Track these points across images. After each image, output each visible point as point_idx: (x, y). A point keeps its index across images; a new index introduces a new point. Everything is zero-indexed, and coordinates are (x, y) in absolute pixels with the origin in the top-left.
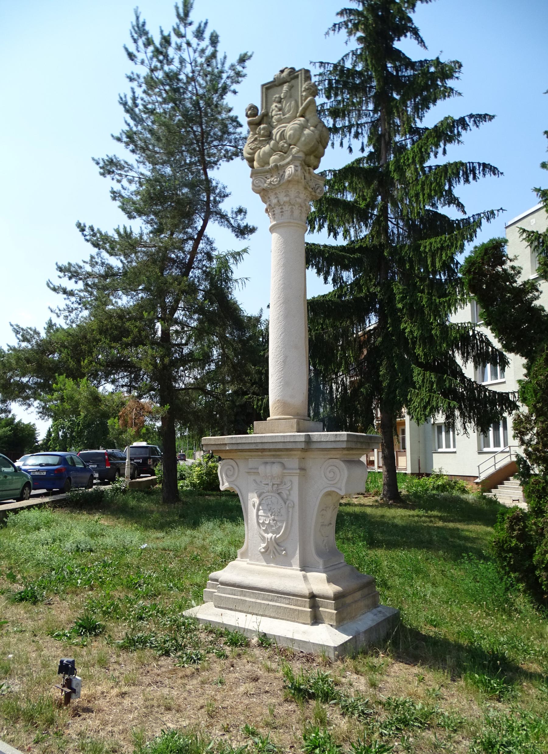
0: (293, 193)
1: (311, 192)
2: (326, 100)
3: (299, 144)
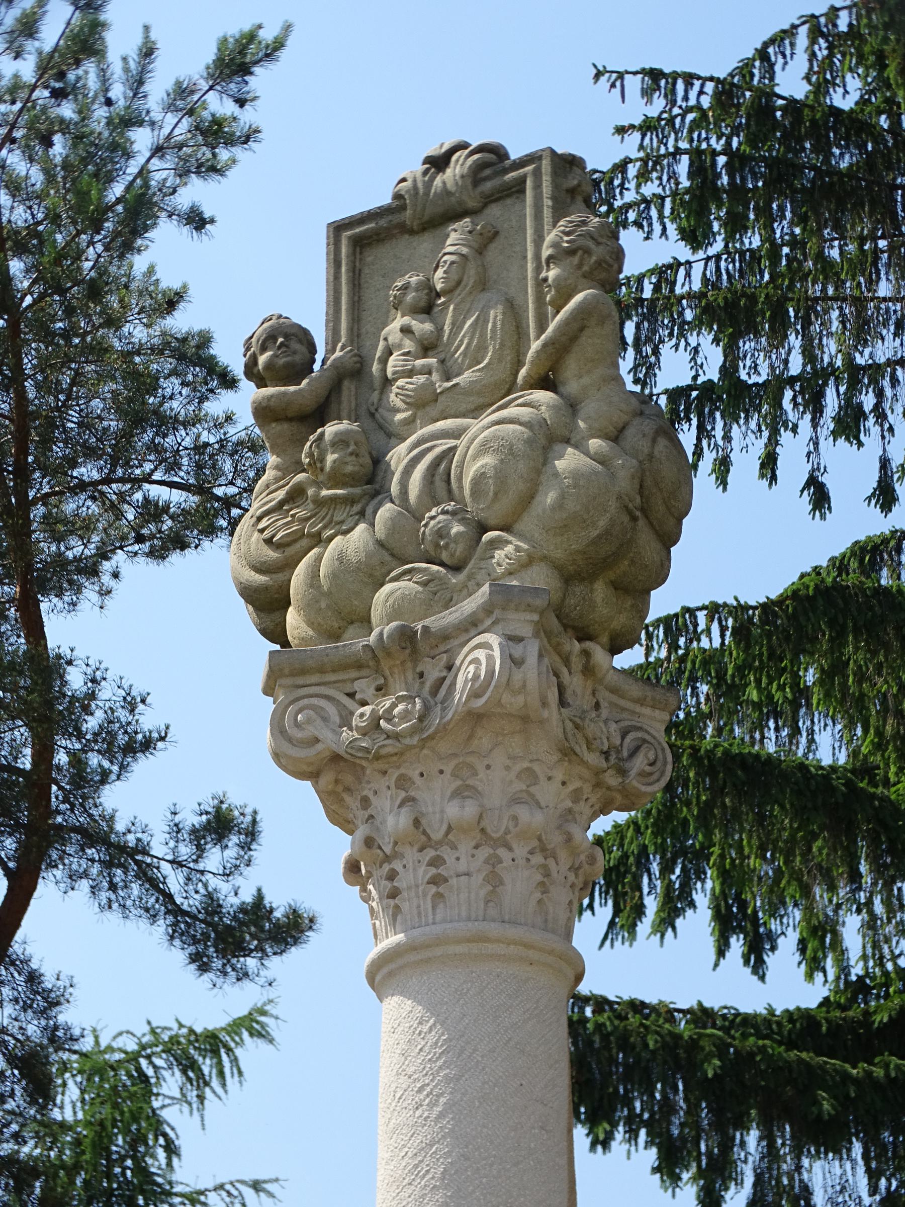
0: (496, 780)
1: (598, 772)
2: (683, 252)
3: (527, 523)
